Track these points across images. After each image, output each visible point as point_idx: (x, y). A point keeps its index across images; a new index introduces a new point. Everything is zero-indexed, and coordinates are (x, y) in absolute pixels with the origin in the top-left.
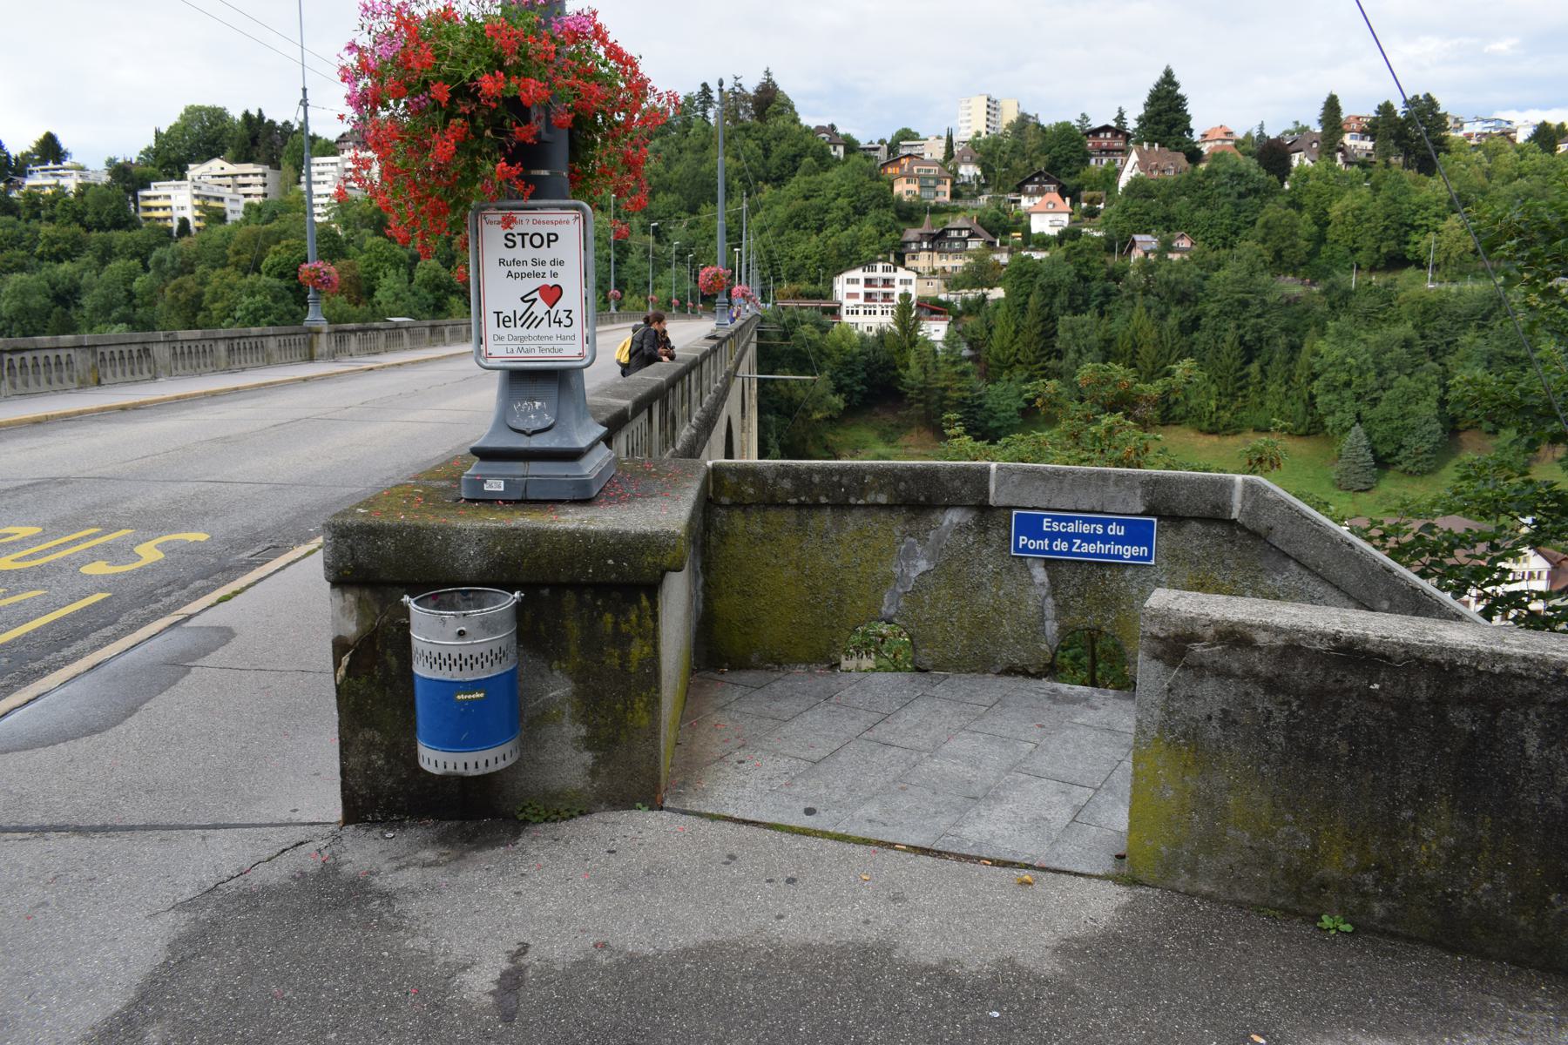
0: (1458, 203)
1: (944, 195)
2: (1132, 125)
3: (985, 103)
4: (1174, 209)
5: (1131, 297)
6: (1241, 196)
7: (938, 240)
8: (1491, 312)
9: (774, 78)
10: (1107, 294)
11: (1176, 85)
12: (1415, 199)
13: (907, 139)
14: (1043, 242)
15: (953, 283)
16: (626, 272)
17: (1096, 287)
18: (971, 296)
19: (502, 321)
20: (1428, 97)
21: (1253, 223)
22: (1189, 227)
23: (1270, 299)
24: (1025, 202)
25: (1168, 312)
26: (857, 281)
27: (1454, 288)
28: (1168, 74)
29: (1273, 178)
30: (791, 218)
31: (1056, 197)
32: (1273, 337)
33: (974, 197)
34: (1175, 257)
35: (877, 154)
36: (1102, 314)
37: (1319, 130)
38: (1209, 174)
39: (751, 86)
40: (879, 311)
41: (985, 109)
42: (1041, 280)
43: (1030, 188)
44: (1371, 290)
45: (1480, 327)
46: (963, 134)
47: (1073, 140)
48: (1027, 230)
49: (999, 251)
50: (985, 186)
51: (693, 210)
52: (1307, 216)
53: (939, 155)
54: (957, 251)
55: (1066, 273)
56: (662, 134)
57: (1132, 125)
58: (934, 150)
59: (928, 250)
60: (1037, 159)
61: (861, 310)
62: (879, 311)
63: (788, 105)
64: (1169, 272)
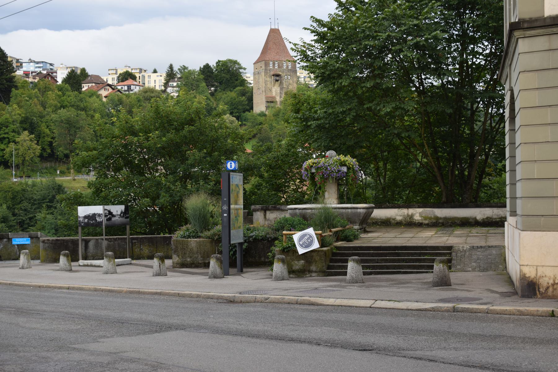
0: (29, 125)
27: (30, 181)
45: (49, 207)
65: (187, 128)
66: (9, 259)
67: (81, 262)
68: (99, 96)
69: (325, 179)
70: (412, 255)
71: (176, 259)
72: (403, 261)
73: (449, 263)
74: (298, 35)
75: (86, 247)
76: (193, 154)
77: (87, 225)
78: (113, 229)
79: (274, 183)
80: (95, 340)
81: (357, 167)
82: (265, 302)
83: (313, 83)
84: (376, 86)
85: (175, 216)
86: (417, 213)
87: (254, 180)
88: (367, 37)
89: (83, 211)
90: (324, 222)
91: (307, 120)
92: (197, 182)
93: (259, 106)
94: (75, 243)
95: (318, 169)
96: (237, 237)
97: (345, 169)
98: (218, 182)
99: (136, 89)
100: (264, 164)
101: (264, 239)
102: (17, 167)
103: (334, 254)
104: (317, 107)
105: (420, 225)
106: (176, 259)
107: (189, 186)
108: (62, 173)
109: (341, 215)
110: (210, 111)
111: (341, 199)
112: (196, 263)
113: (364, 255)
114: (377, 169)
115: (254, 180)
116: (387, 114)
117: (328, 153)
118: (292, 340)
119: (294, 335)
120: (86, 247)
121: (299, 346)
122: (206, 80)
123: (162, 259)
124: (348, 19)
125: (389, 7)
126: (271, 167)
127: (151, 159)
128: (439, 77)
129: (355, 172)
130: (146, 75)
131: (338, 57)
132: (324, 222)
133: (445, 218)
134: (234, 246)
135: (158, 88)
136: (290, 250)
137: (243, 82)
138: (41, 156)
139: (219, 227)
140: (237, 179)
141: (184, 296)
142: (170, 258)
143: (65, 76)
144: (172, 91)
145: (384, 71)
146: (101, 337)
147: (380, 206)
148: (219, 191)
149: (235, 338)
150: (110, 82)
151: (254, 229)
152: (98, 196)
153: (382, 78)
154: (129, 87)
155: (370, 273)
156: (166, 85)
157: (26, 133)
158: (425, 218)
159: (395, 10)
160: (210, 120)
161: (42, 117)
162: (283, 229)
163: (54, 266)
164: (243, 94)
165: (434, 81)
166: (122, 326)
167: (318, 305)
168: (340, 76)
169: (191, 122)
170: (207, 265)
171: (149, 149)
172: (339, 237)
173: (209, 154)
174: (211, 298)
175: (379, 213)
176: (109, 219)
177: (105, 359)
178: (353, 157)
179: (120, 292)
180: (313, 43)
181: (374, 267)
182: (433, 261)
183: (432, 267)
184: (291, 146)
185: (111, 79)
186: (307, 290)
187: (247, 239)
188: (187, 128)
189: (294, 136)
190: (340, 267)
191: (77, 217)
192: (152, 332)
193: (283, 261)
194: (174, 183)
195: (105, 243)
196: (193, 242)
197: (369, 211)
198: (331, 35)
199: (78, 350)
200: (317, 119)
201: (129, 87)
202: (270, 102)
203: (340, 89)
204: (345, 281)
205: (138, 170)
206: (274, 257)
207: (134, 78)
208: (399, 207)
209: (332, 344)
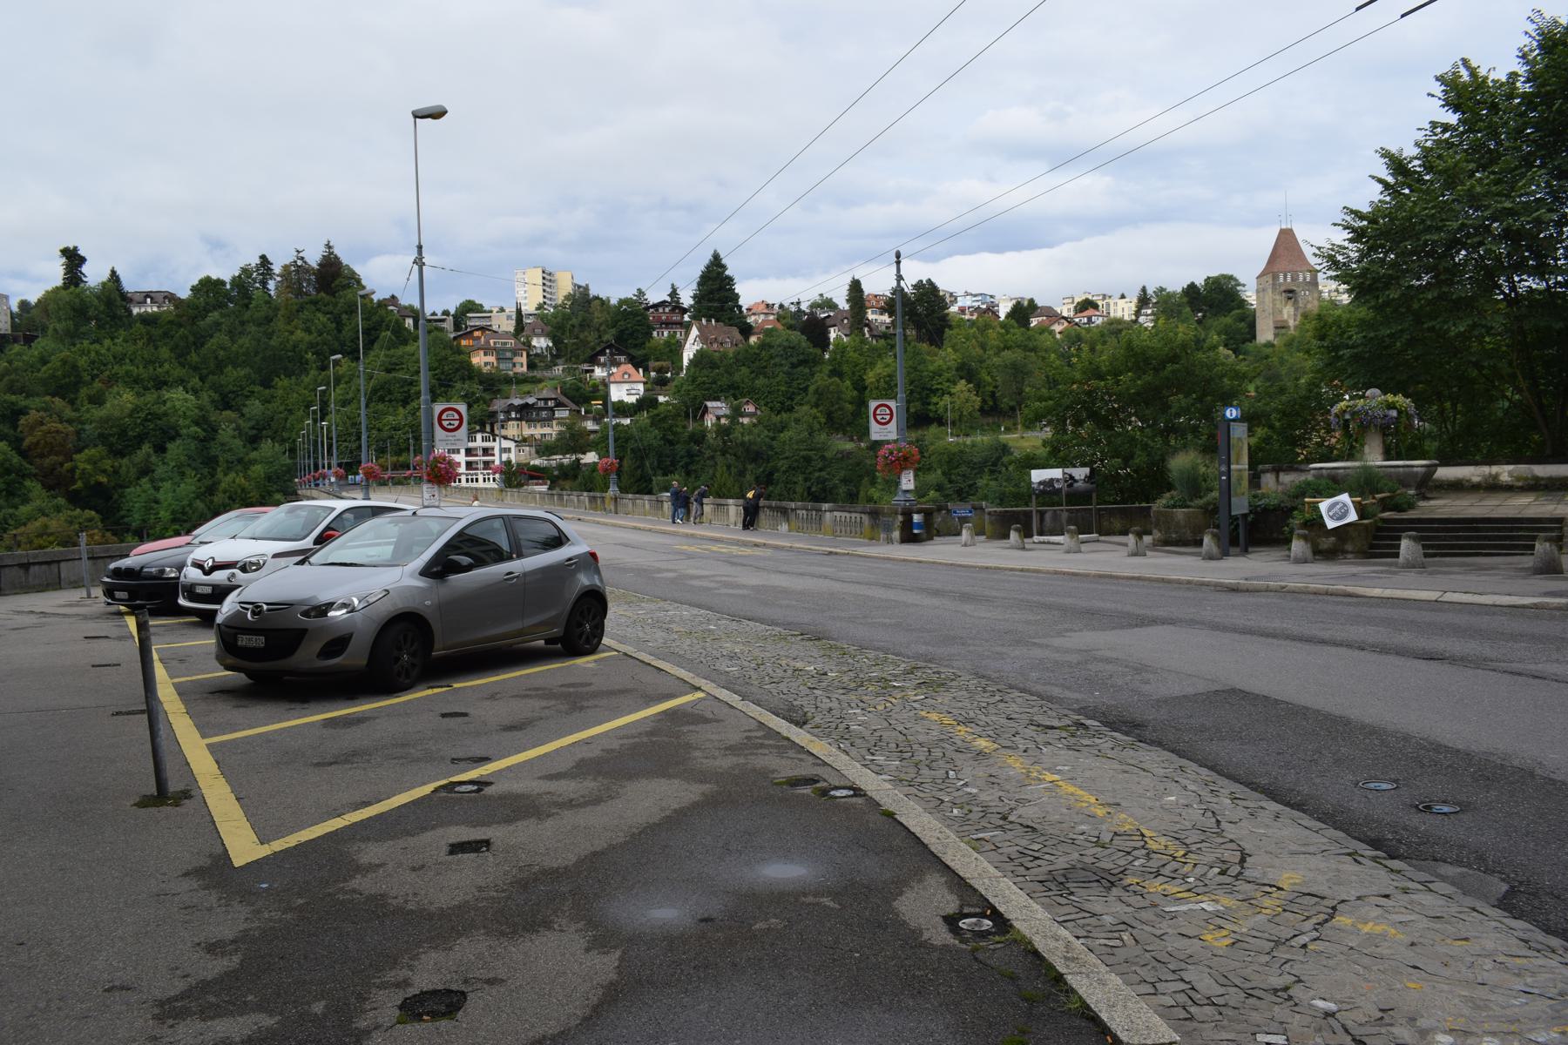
0: (966, 372)
1: (521, 364)
2: (687, 300)
4: (737, 377)
5: (712, 458)
6: (793, 366)
9: (336, 251)
11: (724, 267)
12: (931, 368)
13: (470, 311)
14: (621, 409)
15: (545, 449)
16: (215, 450)
18: (566, 461)
20: (929, 281)
21: (806, 389)
22: (753, 394)
23: (828, 455)
24: (599, 372)
27: (969, 441)
29: (818, 351)
31: (629, 368)
32: (835, 487)
33: (548, 367)
34: (746, 421)
35: (444, 325)
36: (688, 473)
37: (847, 307)
38: (763, 346)
39: (314, 258)
40: (481, 478)
41: (540, 281)
42: (632, 444)
43: (602, 359)
45: (992, 472)
46: (529, 307)
48: (605, 397)
49: (585, 418)
52: (848, 383)
53: (510, 326)
56: (221, 306)
57: (687, 300)
60: (605, 332)
62: (481, 478)
65: (1169, 367)
66: (949, 534)
67: (1036, 538)
68: (1052, 333)
69: (1364, 428)
70: (1499, 529)
71: (1157, 534)
72: (1485, 538)
73: (1558, 541)
74: (1322, 235)
75: (1042, 520)
76: (1178, 400)
77: (1043, 492)
78: (1073, 496)
79: (1289, 432)
80: (1060, 634)
81: (1412, 410)
82: (1282, 591)
83: (1345, 299)
84: (1441, 297)
85: (1154, 481)
86: (1505, 472)
87: (1261, 432)
88: (1428, 229)
89: (1037, 476)
90: (1363, 485)
91: (1336, 348)
92: (1183, 436)
93: (1265, 334)
94: (1028, 515)
95: (1353, 414)
96: (1240, 506)
97: (1394, 413)
98: (1212, 436)
99: (1099, 321)
100: (1276, 410)
101: (1277, 508)
102: (953, 423)
103: (1379, 529)
104: (1353, 331)
105: (1509, 489)
106: (1157, 534)
107: (1173, 442)
108: (1008, 430)
109: (1390, 476)
110: (1199, 343)
111: (1388, 455)
112: (1186, 540)
113: (1423, 530)
114: (1442, 411)
115: (1261, 432)
116: (1460, 334)
117: (1368, 393)
118: (1323, 642)
119: (1326, 635)
120: (1042, 520)
121: (1333, 650)
122: (1190, 303)
123: (1139, 535)
124: (1400, 207)
125: (1463, 184)
126: (1284, 414)
127: (1122, 409)
128: (1542, 278)
129: (1409, 417)
130: (1111, 302)
131: (1383, 260)
132: (1363, 485)
133: (1550, 479)
134: (1236, 518)
135: (1126, 318)
136: (1316, 523)
137: (1242, 303)
138: (982, 410)
139: (1215, 494)
140: (1239, 432)
141: (1169, 582)
142: (1150, 533)
143: (1008, 310)
144: (1146, 321)
145: (1455, 275)
146: (1067, 630)
147: (1447, 462)
148: (1216, 445)
149: (1243, 637)
150: (1065, 314)
151: (1264, 496)
152: (1056, 456)
153: (1452, 283)
154: (1089, 318)
155: (1435, 555)
156: (1138, 313)
157: (963, 382)
158: (1518, 479)
159: (1473, 187)
160: (1200, 355)
161: (982, 362)
162: (1304, 495)
163: (1003, 543)
164: (1242, 319)
165: (1532, 283)
166: (1093, 617)
167: (1357, 596)
168: (1387, 286)
169: (1174, 359)
170: (1200, 543)
171: (1119, 395)
172: (1385, 505)
173: (1200, 400)
174: (1207, 584)
175: (1445, 473)
176: (1070, 486)
177: (1074, 658)
178: (1406, 396)
179: (1087, 575)
180: (1346, 244)
181: (1439, 547)
182: (1534, 538)
183: (1532, 547)
184: (1314, 385)
185: (1066, 310)
186: (1341, 577)
187: (1254, 509)
188: (1169, 367)
189: (1318, 371)
190: (1389, 546)
191: (1031, 482)
192: (1131, 626)
193: (1305, 538)
194: (1152, 438)
195: (1065, 515)
196: (1180, 513)
197: (1431, 469)
198: (1372, 230)
199: (1040, 646)
200: (1353, 347)
201: (1089, 318)
202: (1280, 327)
203: (1387, 303)
204: (1396, 565)
205: (1104, 423)
206: (1291, 532)
207: (1095, 306)
208: (1476, 464)
209: (1384, 650)
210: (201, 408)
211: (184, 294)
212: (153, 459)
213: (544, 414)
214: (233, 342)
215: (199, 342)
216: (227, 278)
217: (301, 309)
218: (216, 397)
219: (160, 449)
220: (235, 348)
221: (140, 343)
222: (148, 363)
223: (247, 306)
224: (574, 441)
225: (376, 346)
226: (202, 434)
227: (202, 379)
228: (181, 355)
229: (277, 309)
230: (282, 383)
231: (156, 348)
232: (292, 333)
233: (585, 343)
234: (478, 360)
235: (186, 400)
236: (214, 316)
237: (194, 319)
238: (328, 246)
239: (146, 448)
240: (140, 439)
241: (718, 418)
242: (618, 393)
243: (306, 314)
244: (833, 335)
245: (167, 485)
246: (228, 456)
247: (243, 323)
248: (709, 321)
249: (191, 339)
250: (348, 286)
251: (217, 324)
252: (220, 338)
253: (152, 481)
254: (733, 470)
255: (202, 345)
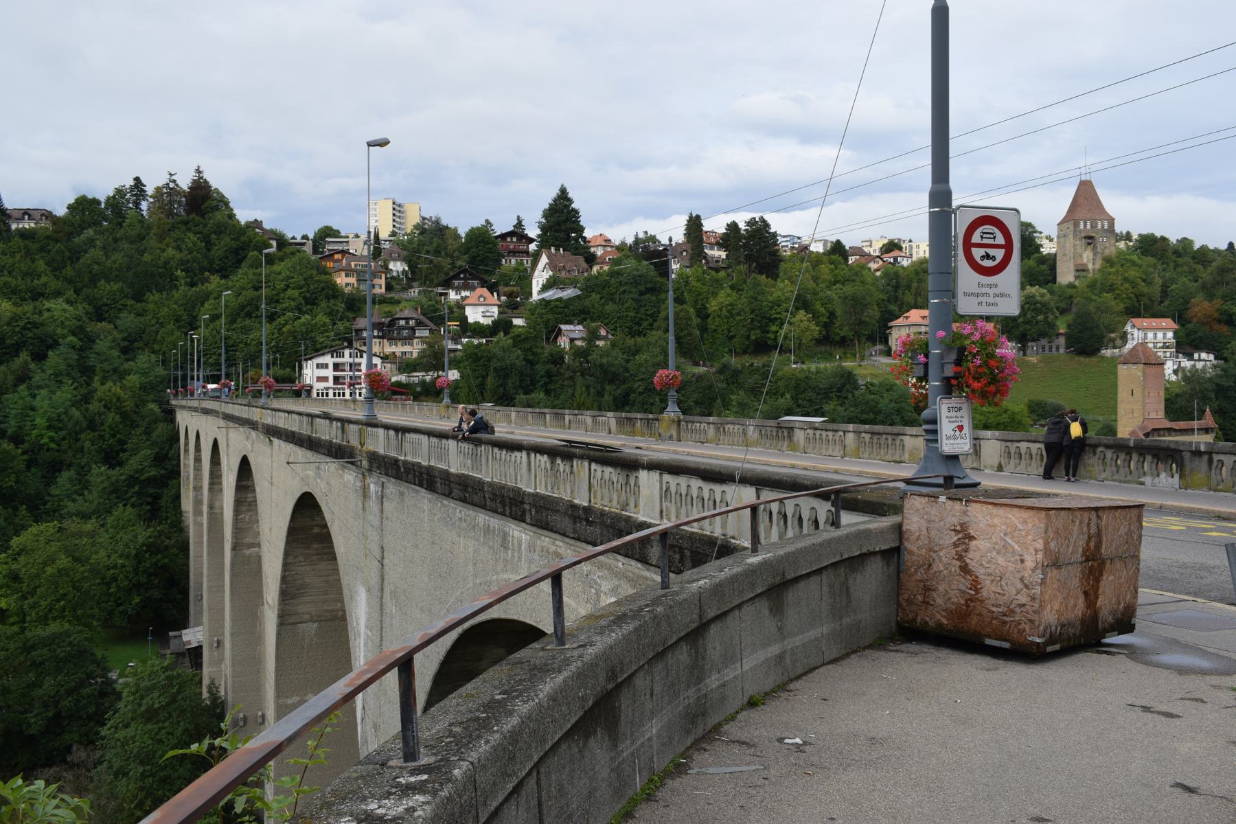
0: (803, 303)
2: (533, 232)
3: (391, 206)
5: (571, 378)
7: (388, 330)
8: (843, 385)
9: (206, 176)
10: (549, 375)
11: (570, 201)
13: (330, 236)
14: (478, 330)
15: (407, 366)
16: (92, 360)
17: (540, 369)
18: (428, 378)
19: (948, 438)
24: (453, 295)
25: (603, 389)
26: (326, 366)
28: (563, 191)
30: (243, 307)
31: (484, 291)
33: (406, 289)
34: (601, 343)
35: (305, 248)
39: (185, 183)
41: (391, 211)
42: (495, 364)
43: (456, 282)
44: (753, 370)
47: (488, 243)
48: (464, 319)
50: (413, 280)
51: (138, 297)
54: (405, 338)
55: (516, 357)
56: (96, 223)
57: (533, 232)
58: (358, 248)
59: (378, 337)
60: (458, 258)
61: (331, 392)
63: (223, 201)
64: (601, 356)
93: (1065, 276)
161: (815, 294)
201: (896, 259)
202: (1081, 270)
210: (78, 319)
211: (61, 211)
212: (33, 366)
213: (405, 333)
214: (107, 257)
215: (75, 255)
216: (102, 198)
217: (172, 228)
218: (90, 309)
219: (40, 357)
220: (108, 263)
221: (18, 256)
222: (25, 275)
223: (120, 225)
224: (433, 359)
225: (243, 264)
226: (79, 344)
227: (77, 292)
228: (56, 267)
229: (149, 228)
230: (153, 297)
231: (33, 262)
232: (164, 251)
233: (439, 268)
234: (341, 280)
235: (65, 310)
236: (90, 232)
237: (70, 235)
238: (198, 171)
239: (24, 356)
240: (17, 349)
241: (572, 340)
242: (474, 315)
243: (176, 234)
244: (675, 266)
245: (44, 392)
246: (105, 366)
247: (116, 240)
248: (557, 249)
249: (67, 254)
250: (217, 208)
251: (91, 241)
252: (94, 253)
253: (29, 388)
254: (592, 390)
255: (78, 259)
